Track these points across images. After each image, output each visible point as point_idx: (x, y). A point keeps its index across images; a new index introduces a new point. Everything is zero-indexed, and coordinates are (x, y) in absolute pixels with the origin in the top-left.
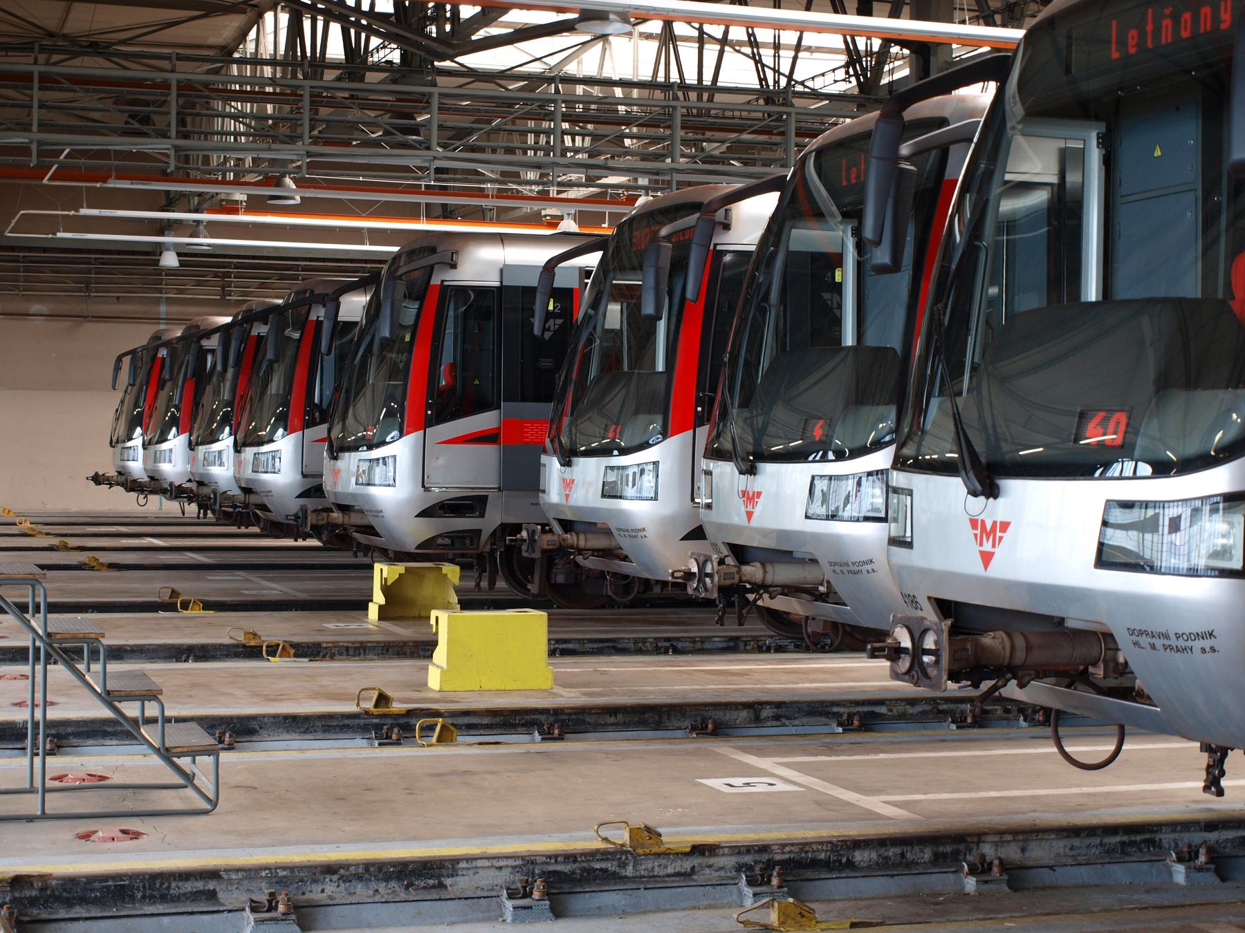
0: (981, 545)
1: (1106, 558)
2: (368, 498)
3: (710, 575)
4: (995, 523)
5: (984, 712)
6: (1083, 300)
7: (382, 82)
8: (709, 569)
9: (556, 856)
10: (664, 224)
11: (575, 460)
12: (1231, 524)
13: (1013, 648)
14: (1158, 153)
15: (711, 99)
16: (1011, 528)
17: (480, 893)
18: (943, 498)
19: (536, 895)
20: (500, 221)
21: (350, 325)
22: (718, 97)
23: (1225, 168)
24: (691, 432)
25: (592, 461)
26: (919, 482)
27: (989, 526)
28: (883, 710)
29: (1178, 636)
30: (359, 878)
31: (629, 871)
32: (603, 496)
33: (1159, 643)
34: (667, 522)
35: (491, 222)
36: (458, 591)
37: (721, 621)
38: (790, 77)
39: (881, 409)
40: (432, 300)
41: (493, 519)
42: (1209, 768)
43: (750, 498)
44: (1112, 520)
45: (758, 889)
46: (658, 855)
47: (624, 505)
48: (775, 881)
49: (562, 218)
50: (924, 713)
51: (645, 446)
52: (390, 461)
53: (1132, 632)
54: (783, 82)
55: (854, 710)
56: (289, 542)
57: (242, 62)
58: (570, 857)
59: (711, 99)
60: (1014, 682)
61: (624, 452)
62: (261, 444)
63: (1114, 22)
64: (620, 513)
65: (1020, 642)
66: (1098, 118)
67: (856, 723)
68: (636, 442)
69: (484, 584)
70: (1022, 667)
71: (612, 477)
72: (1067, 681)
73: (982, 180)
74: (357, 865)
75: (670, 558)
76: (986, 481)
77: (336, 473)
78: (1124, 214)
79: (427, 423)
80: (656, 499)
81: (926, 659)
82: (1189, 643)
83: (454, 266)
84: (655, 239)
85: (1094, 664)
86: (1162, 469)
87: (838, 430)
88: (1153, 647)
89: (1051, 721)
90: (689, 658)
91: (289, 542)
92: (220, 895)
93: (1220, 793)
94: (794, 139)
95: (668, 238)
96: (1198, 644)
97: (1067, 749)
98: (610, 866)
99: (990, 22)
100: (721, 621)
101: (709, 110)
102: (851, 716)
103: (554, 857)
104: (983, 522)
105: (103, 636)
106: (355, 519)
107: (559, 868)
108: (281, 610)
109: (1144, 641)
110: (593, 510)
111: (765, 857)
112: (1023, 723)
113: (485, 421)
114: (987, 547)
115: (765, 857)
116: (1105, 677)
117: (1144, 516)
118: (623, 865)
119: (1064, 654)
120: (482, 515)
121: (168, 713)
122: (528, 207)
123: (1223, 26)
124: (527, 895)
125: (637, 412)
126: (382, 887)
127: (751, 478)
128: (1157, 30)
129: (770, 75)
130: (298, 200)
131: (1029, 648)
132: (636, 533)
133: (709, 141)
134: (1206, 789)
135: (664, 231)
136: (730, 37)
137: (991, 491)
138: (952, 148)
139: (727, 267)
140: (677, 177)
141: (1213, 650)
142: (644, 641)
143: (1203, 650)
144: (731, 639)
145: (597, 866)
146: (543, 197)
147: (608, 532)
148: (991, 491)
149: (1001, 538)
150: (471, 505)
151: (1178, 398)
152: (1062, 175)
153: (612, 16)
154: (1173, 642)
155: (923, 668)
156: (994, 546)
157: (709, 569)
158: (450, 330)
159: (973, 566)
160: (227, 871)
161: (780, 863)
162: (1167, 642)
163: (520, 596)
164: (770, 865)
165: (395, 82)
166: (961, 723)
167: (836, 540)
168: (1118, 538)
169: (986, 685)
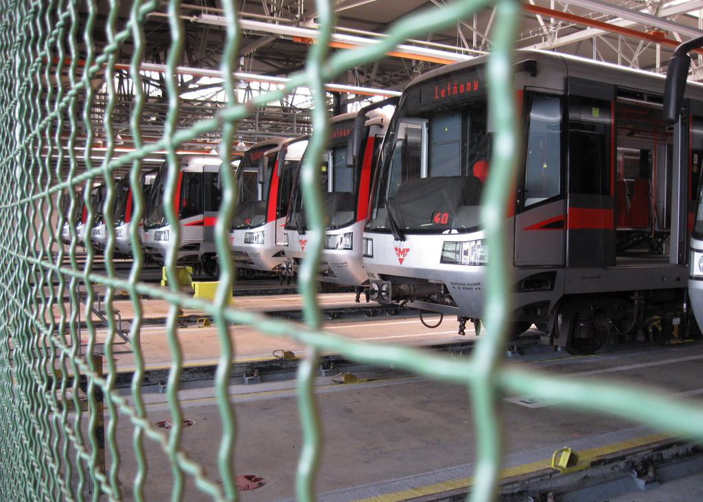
1: (444, 260)
2: (159, 245)
3: (291, 269)
5: (376, 311)
6: (422, 177)
7: (156, 102)
8: (290, 266)
9: (261, 362)
10: (265, 151)
12: (484, 248)
13: (410, 290)
14: (446, 130)
15: (264, 110)
16: (410, 251)
17: (235, 375)
18: (384, 243)
19: (255, 375)
20: (189, 151)
21: (147, 185)
22: (266, 109)
24: (275, 221)
25: (240, 231)
26: (375, 236)
27: (402, 250)
28: (343, 311)
30: (196, 372)
31: (284, 366)
32: (245, 242)
33: (461, 287)
34: (268, 251)
35: (186, 151)
36: (192, 276)
37: (281, 284)
38: (291, 105)
39: (350, 212)
41: (202, 251)
42: (460, 327)
44: (446, 249)
45: (327, 370)
46: (293, 360)
47: (252, 245)
48: (331, 368)
49: (211, 150)
50: (357, 312)
51: (260, 225)
52: (167, 232)
53: (452, 283)
54: (289, 106)
55: (335, 311)
56: (123, 260)
57: (101, 94)
58: (265, 362)
59: (264, 110)
60: (409, 301)
61: (252, 228)
62: (159, 227)
63: (436, 88)
64: (251, 248)
65: (412, 288)
66: (427, 118)
67: (336, 316)
68: (256, 224)
69: (197, 273)
70: (413, 296)
71: (248, 236)
73: (390, 138)
74: (196, 368)
75: (270, 264)
76: (401, 235)
77: (147, 236)
78: (434, 149)
81: (383, 294)
83: (187, 165)
84: (262, 156)
85: (434, 294)
86: (461, 231)
87: (334, 220)
88: (459, 288)
89: (422, 313)
90: (275, 296)
91: (123, 260)
92: (150, 380)
93: (464, 334)
94: (295, 124)
95: (267, 156)
96: (474, 287)
97: (424, 321)
98: (278, 365)
99: (361, 85)
100: (281, 284)
101: (263, 113)
102: (334, 314)
103: (260, 363)
105: (98, 292)
106: (154, 252)
107: (261, 366)
109: (456, 286)
110: (240, 247)
111: (327, 360)
112: (387, 314)
113: (199, 218)
114: (401, 257)
115: (327, 360)
116: (438, 298)
118: (282, 364)
119: (425, 291)
120: (198, 250)
121: (122, 318)
122: (199, 146)
124: (252, 375)
125: (256, 214)
126: (203, 374)
127: (303, 236)
128: (451, 91)
129: (285, 104)
130: (122, 143)
131: (415, 289)
132: (256, 255)
133: (264, 124)
134: (459, 333)
135: (266, 153)
136: (270, 89)
137: (403, 239)
138: (371, 127)
139: (286, 166)
140: (257, 136)
142: (257, 291)
144: (286, 289)
145: (274, 365)
146: (205, 142)
147: (246, 255)
148: (403, 239)
150: (195, 246)
151: (340, 213)
152: (406, 136)
153: (242, 81)
155: (382, 296)
157: (290, 266)
159: (398, 264)
160: (152, 371)
161: (332, 361)
163: (209, 277)
164: (329, 362)
165: (160, 102)
166: (369, 315)
168: (447, 255)
169: (401, 302)
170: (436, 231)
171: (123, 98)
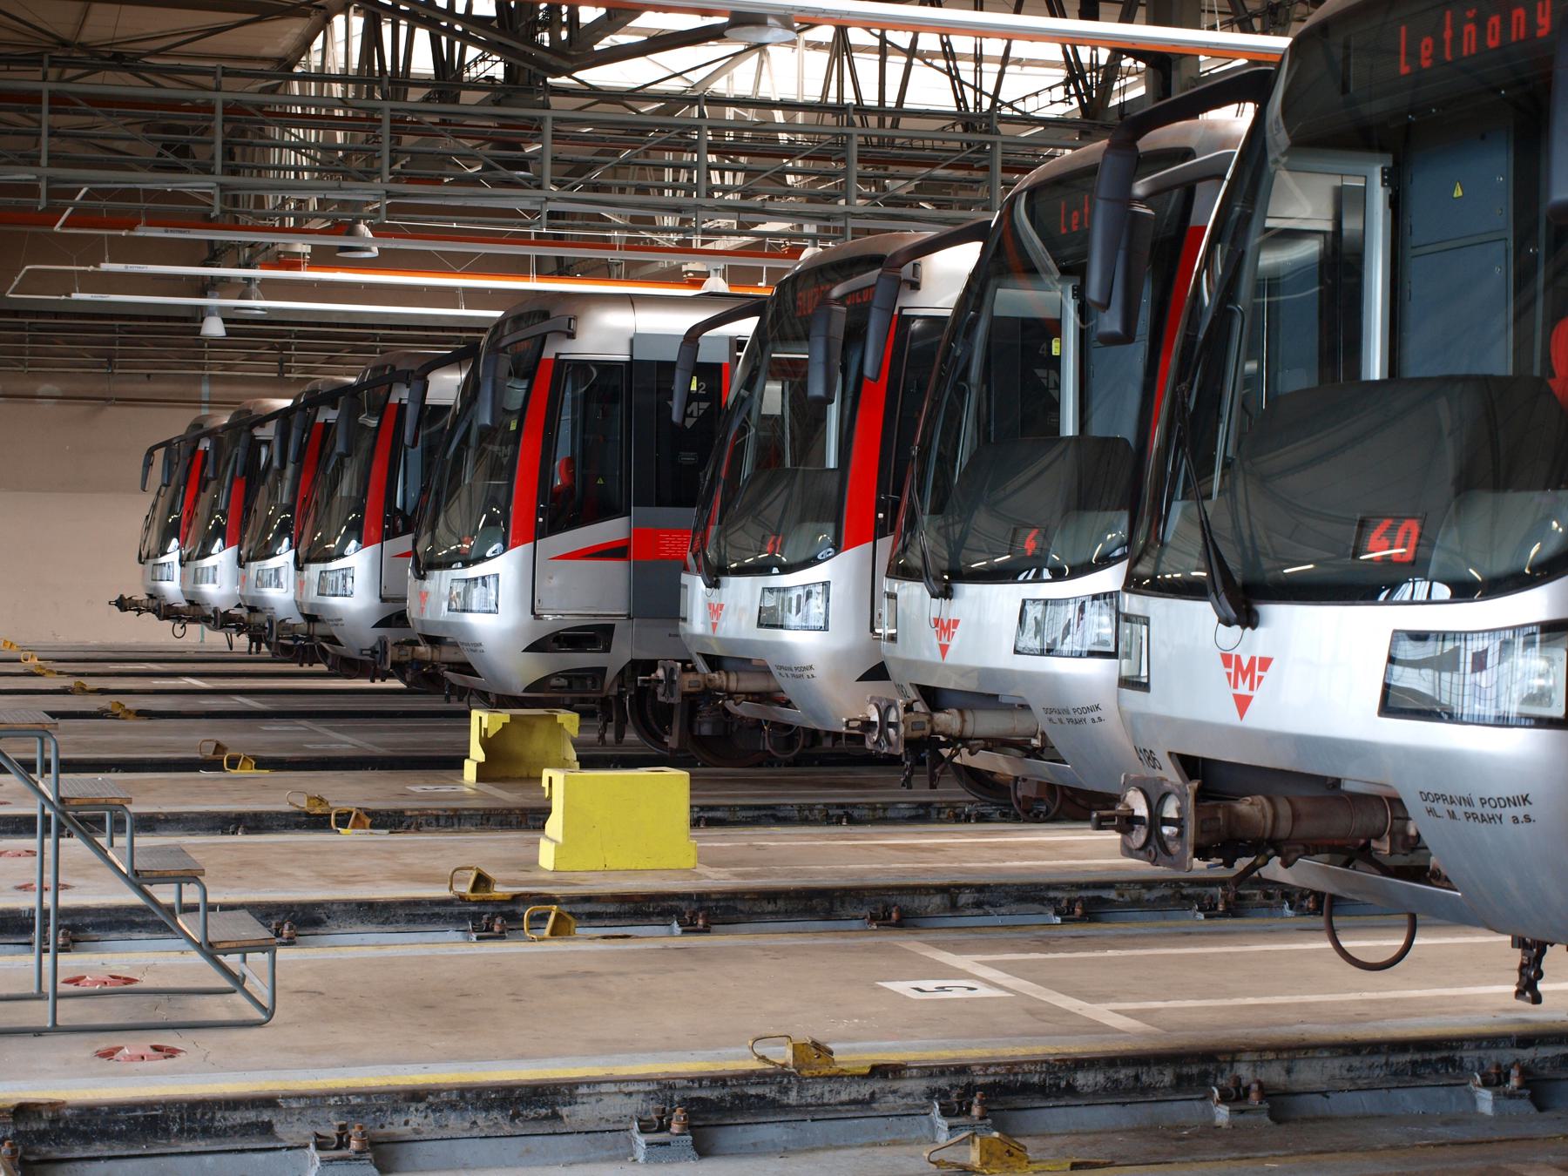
0: (1236, 686)
1: (1392, 704)
2: (463, 628)
3: (894, 725)
4: (1253, 659)
5: (1240, 897)
6: (1364, 378)
7: (481, 103)
8: (892, 718)
9: (700, 1079)
10: (836, 283)
11: (724, 579)
12: (1550, 661)
13: (1275, 817)
14: (1458, 193)
15: (895, 125)
16: (1273, 666)
17: (604, 1126)
18: (1188, 628)
19: (675, 1128)
20: (629, 279)
21: (441, 410)
22: (905, 123)
23: (1543, 211)
24: (870, 544)
25: (745, 581)
26: (1158, 608)
27: (1245, 664)
28: (1112, 895)
29: (1483, 802)
30: (453, 1106)
31: (792, 1098)
32: (760, 625)
33: (1460, 810)
34: (840, 658)
35: (619, 280)
36: (577, 744)
37: (908, 783)
38: (995, 97)
39: (1110, 516)
40: (544, 378)
41: (621, 654)
42: (1523, 968)
43: (945, 627)
44: (1400, 655)
45: (955, 1121)
46: (829, 1078)
47: (786, 636)
48: (976, 1111)
49: (707, 274)
50: (1163, 898)
51: (812, 562)
52: (492, 581)
53: (1425, 796)
54: (986, 103)
55: (1075, 895)
56: (365, 684)
57: (305, 78)
58: (718, 1080)
59: (895, 125)
60: (1277, 860)
61: (786, 569)
62: (328, 559)
63: (1403, 28)
64: (781, 647)
65: (1284, 809)
66: (1382, 149)
67: (1078, 911)
68: (801, 557)
69: (610, 736)
70: (1288, 840)
71: (770, 601)
72: (1344, 858)
73: (1236, 227)
74: (450, 1090)
75: (844, 704)
76: (1242, 606)
77: (423, 596)
78: (1416, 270)
79: (538, 533)
80: (826, 629)
81: (1166, 830)
82: (1498, 811)
83: (571, 336)
84: (825, 301)
85: (1378, 837)
86: (1464, 591)
87: (1056, 542)
88: (1452, 815)
89: (1323, 909)
90: (868, 829)
91: (365, 684)
92: (278, 1128)
93: (1537, 999)
94: (1000, 176)
95: (841, 300)
96: (1509, 812)
97: (1344, 944)
98: (769, 1091)
99: (1246, 28)
100: (908, 783)
101: (893, 138)
102: (1071, 903)
103: (698, 1080)
104: (1238, 658)
105: (130, 801)
106: (447, 654)
107: (704, 1094)
108: (354, 769)
109: (1441, 807)
110: (747, 643)
111: (963, 1080)
112: (1288, 912)
113: (611, 530)
114: (1243, 689)
115: (963, 1080)
116: (1392, 853)
117: (1441, 651)
118: (785, 1090)
119: (1340, 824)
120: (607, 649)
121: (211, 899)
122: (665, 261)
123: (1540, 33)
124: (663, 1128)
125: (802, 520)
126: (481, 1118)
127: (945, 602)
128: (1457, 38)
129: (969, 94)
130: (375, 252)
131: (1296, 817)
132: (800, 672)
133: (893, 177)
134: (1519, 994)
135: (836, 292)
136: (920, 47)
137: (1249, 619)
138: (1199, 186)
139: (916, 336)
140: (853, 223)
141: (1528, 819)
142: (811, 807)
143: (1515, 820)
144: (921, 805)
145: (752, 1091)
146: (684, 248)
147: (765, 671)
148: (1249, 619)
149: (1260, 678)
150: (593, 636)
152: (1338, 221)
153: (770, 21)
154: (1478, 809)
155: (1162, 842)
156: (1251, 688)
157: (892, 718)
158: (566, 417)
159: (1226, 714)
160: (286, 1097)
161: (982, 1087)
162: (1469, 810)
163: (655, 751)
164: (970, 1090)
165: (497, 103)
166: (1210, 911)
167: (1053, 680)
168: (1408, 679)
169: (1242, 863)
170: (762, 569)
171: (873, 120)
